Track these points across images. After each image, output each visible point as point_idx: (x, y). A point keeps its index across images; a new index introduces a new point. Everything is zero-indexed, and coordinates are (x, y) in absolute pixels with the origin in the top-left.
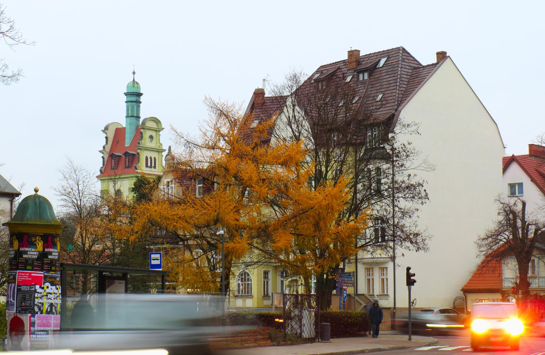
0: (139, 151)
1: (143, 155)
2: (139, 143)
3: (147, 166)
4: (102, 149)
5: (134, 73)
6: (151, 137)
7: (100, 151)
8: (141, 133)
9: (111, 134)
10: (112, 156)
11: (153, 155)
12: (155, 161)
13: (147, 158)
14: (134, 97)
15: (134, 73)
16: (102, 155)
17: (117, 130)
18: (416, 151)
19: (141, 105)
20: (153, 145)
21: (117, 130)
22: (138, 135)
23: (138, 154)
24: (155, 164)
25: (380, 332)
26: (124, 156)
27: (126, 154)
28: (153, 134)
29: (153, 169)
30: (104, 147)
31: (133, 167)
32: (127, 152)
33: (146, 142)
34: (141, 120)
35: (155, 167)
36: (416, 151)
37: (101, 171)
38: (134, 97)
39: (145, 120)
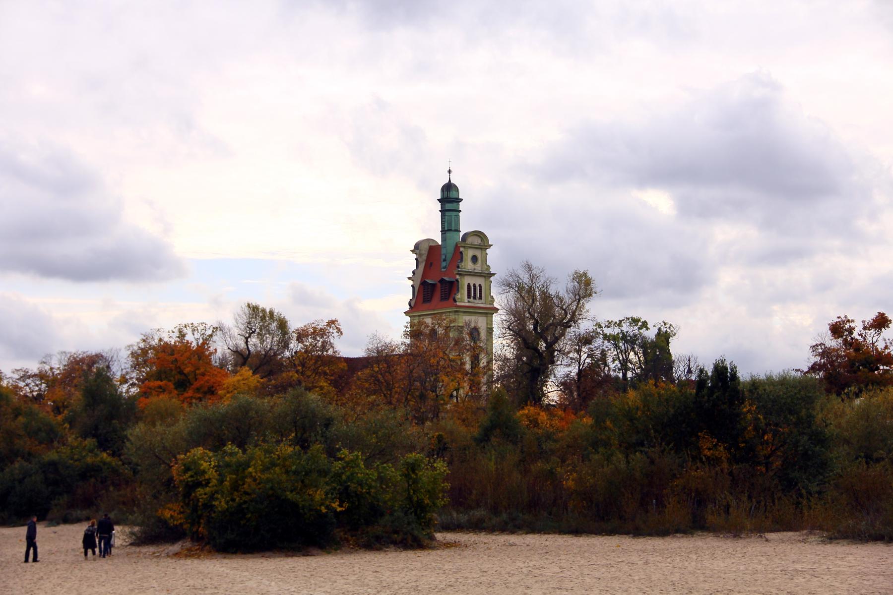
0: (458, 277)
1: (466, 281)
2: (458, 267)
3: (469, 297)
4: (411, 275)
5: (450, 172)
6: (475, 259)
7: (409, 278)
8: (461, 253)
9: (425, 252)
10: (423, 283)
11: (478, 281)
12: (480, 289)
13: (469, 285)
14: (449, 198)
15: (450, 172)
16: (411, 283)
17: (431, 248)
18: (842, 317)
19: (461, 214)
20: (478, 268)
21: (431, 248)
22: (458, 255)
23: (457, 280)
24: (480, 294)
25: (113, 551)
26: (439, 284)
27: (442, 281)
28: (478, 253)
29: (477, 301)
30: (414, 272)
31: (451, 299)
32: (443, 279)
33: (468, 265)
34: (461, 234)
35: (480, 298)
36: (842, 317)
37: (410, 304)
38: (449, 198)
39: (466, 235)
